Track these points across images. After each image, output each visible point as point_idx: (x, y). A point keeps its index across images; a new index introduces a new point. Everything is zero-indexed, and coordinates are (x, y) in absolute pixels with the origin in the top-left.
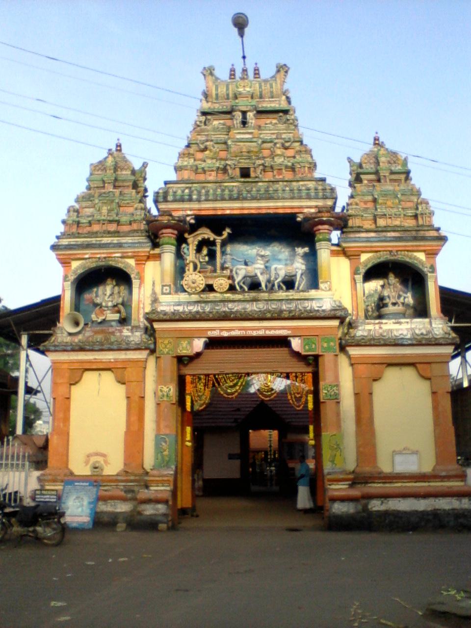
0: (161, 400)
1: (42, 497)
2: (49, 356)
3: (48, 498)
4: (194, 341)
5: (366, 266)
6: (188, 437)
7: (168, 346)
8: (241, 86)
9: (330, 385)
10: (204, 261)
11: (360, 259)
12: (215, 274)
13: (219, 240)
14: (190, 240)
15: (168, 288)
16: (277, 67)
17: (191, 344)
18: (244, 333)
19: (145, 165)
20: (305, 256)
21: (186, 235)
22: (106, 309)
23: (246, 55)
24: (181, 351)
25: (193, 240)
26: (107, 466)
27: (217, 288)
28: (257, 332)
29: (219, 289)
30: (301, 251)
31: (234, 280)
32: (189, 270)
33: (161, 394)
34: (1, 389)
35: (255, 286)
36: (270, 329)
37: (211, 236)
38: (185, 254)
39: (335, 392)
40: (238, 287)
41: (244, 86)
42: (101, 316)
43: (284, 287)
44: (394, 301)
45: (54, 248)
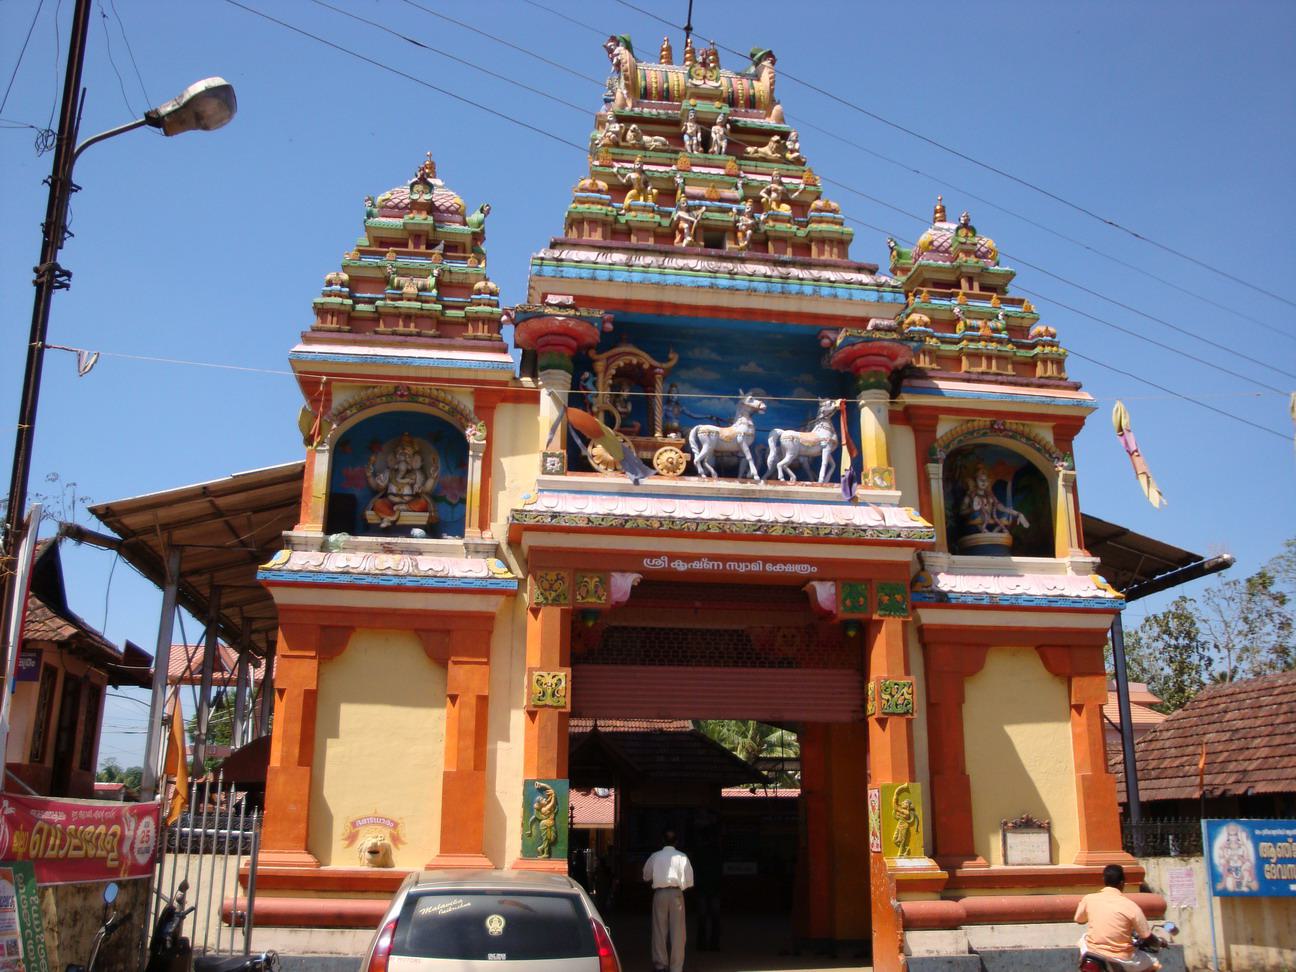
0: (540, 703)
2: (1125, 889)
4: (613, 579)
5: (948, 446)
7: (556, 586)
8: (698, 75)
11: (935, 431)
14: (600, 366)
15: (557, 460)
17: (605, 583)
18: (721, 567)
20: (834, 419)
22: (397, 499)
23: (693, 24)
24: (583, 598)
25: (605, 367)
26: (398, 848)
28: (747, 566)
33: (539, 689)
34: (362, 969)
36: (775, 560)
37: (647, 361)
39: (905, 699)
40: (700, 470)
41: (705, 77)
42: (389, 515)
43: (793, 476)
44: (991, 522)
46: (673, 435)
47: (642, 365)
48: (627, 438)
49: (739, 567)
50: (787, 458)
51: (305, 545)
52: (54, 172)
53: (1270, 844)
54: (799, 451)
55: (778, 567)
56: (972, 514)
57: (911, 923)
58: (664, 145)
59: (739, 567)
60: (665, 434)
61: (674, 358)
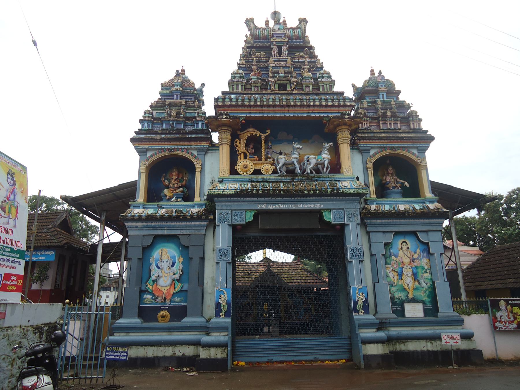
1: (112, 354)
3: (118, 356)
6: (75, 246)
9: (355, 248)
10: (251, 152)
12: (261, 162)
13: (263, 136)
14: (242, 136)
16: (299, 21)
19: (203, 85)
20: (330, 150)
21: (239, 133)
25: (245, 135)
27: (263, 171)
28: (296, 206)
29: (265, 173)
30: (327, 145)
31: (276, 167)
32: (240, 158)
35: (291, 172)
37: (258, 134)
38: (237, 146)
40: (279, 171)
44: (394, 185)
45: (133, 140)
46: (269, 160)
47: (257, 135)
48: (250, 162)
49: (293, 206)
50: (311, 166)
51: (138, 207)
52: (31, 285)
53: (517, 308)
54: (285, 162)
55: (308, 206)
56: (386, 183)
57: (366, 342)
58: (264, 55)
59: (293, 206)
60: (266, 160)
61: (268, 132)
